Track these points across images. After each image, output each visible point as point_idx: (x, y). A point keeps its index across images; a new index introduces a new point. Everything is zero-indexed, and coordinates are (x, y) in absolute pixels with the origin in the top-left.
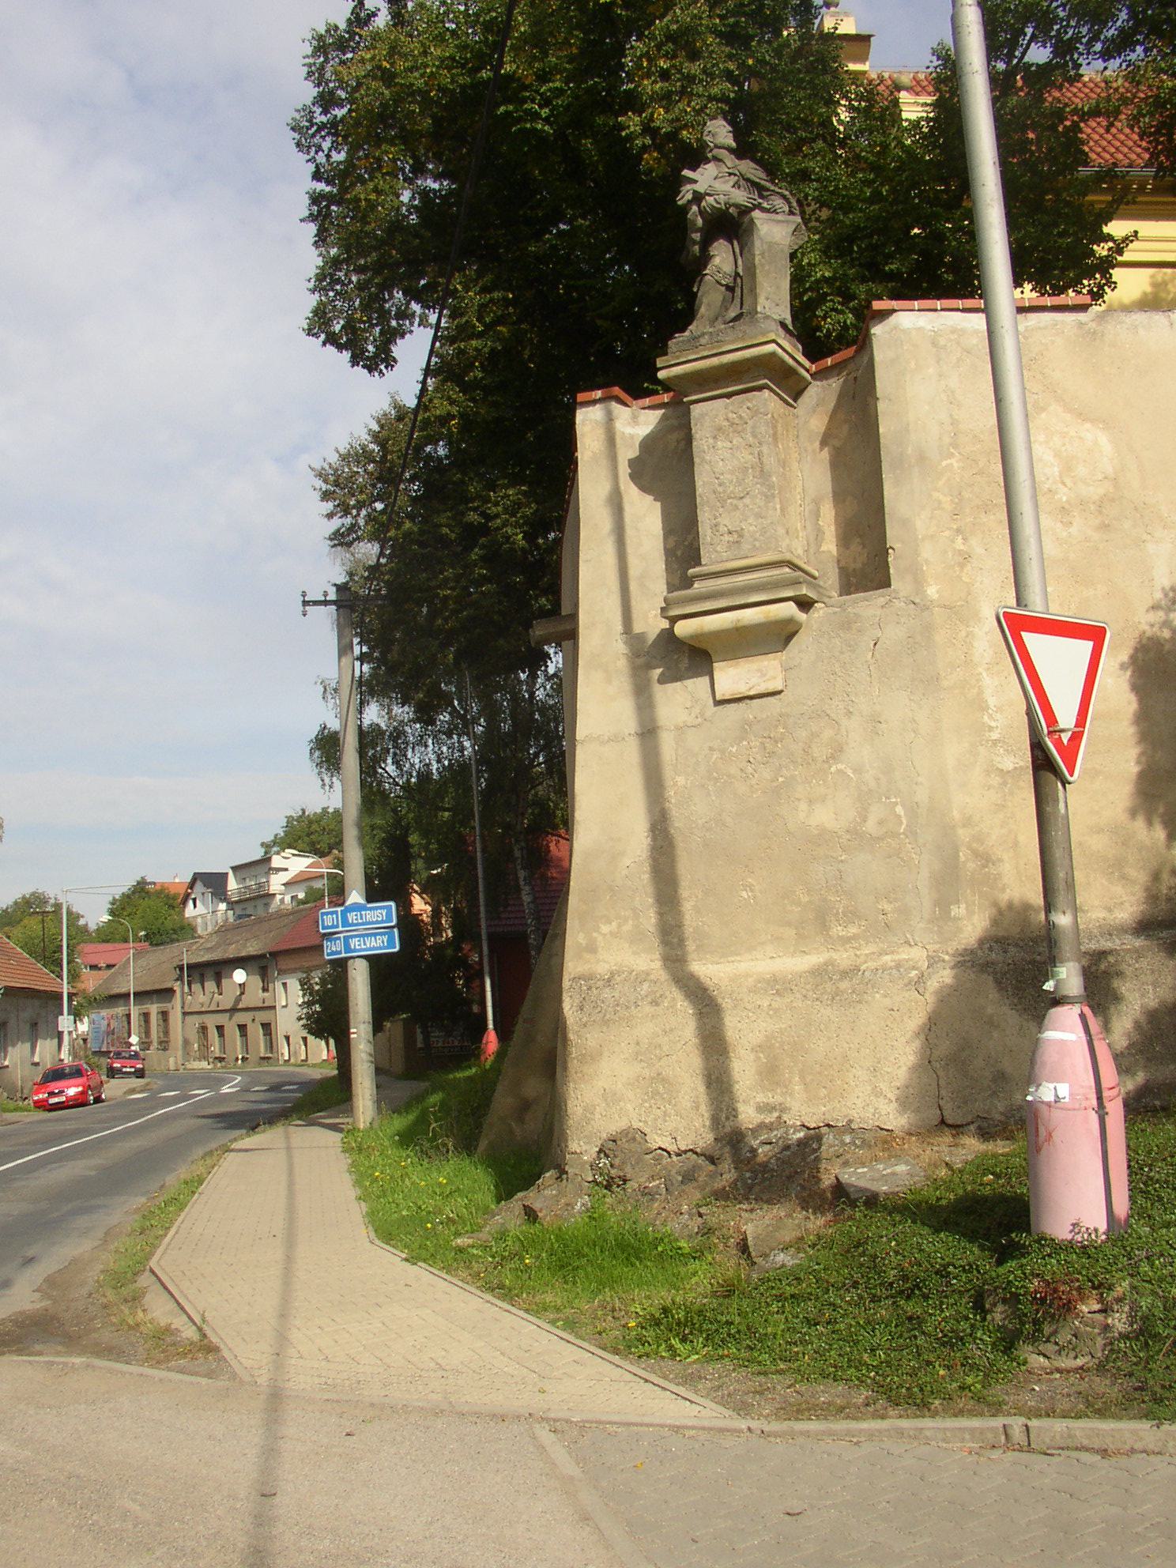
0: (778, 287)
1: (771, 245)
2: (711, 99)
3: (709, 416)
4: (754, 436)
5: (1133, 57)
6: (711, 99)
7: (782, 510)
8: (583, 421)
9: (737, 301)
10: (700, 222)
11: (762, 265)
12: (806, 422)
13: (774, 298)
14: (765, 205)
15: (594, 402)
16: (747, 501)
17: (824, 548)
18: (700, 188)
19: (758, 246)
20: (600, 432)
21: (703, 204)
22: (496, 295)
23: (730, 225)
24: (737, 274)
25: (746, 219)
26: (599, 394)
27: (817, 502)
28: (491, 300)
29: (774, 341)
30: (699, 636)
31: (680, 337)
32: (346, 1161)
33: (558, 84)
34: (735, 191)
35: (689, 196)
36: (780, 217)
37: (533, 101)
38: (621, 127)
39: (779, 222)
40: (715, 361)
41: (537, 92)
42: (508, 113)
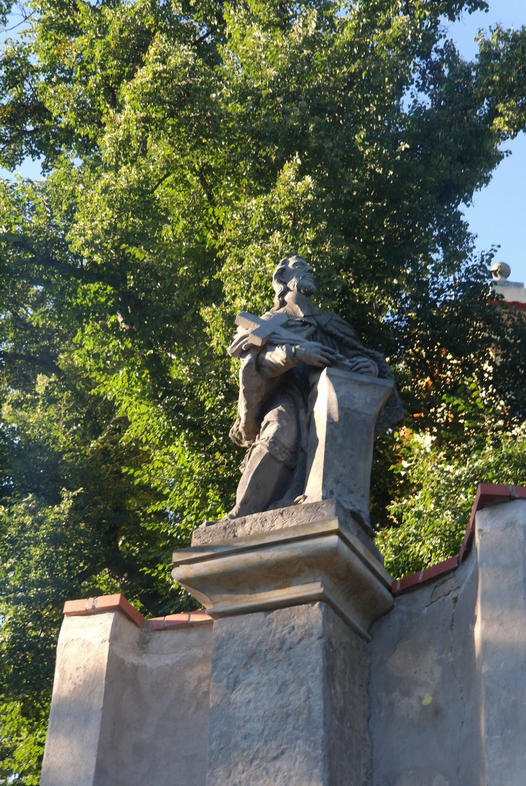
36: (364, 378)
39: (362, 384)
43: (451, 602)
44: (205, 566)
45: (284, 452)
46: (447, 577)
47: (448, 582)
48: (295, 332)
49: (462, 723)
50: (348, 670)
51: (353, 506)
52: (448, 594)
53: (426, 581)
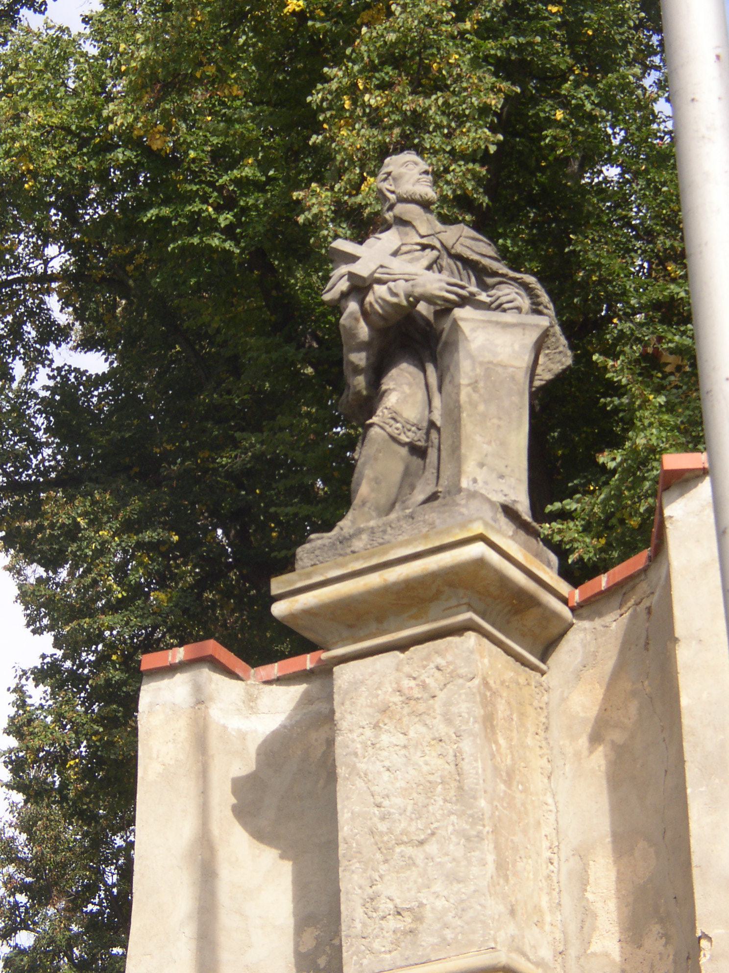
0: (503, 444)
1: (490, 368)
2: (455, 155)
3: (367, 683)
6: (455, 155)
7: (501, 866)
8: (151, 705)
9: (430, 473)
10: (363, 331)
11: (474, 405)
12: (564, 700)
13: (496, 460)
14: (483, 297)
15: (172, 669)
16: (432, 848)
17: (595, 948)
18: (362, 269)
19: (466, 369)
20: (181, 729)
21: (370, 298)
22: (148, 535)
23: (417, 336)
24: (432, 424)
25: (447, 325)
26: (180, 654)
27: (582, 854)
28: (139, 545)
29: (482, 538)
31: (319, 540)
33: (248, 172)
34: (433, 276)
35: (344, 285)
36: (509, 317)
37: (204, 201)
38: (298, 206)
39: (506, 326)
40: (374, 580)
41: (211, 184)
42: (161, 220)
43: (645, 612)
44: (314, 597)
45: (409, 430)
46: (637, 581)
47: (639, 586)
48: (411, 261)
49: (666, 771)
50: (515, 717)
51: (506, 495)
52: (640, 603)
53: (615, 585)
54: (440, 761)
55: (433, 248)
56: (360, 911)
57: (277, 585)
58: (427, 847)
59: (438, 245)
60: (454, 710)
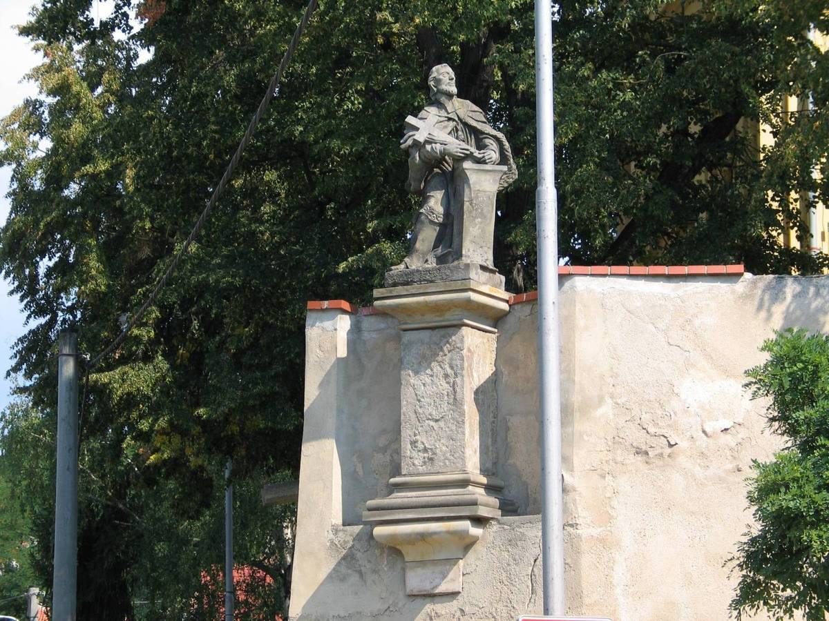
4: (452, 368)
5: (642, 198)
14: (477, 154)
16: (442, 424)
30: (393, 537)
32: (33, 99)
36: (488, 167)
54: (447, 385)
55: (454, 120)
56: (409, 446)
57: (376, 293)
58: (440, 423)
59: (457, 119)
60: (454, 362)
